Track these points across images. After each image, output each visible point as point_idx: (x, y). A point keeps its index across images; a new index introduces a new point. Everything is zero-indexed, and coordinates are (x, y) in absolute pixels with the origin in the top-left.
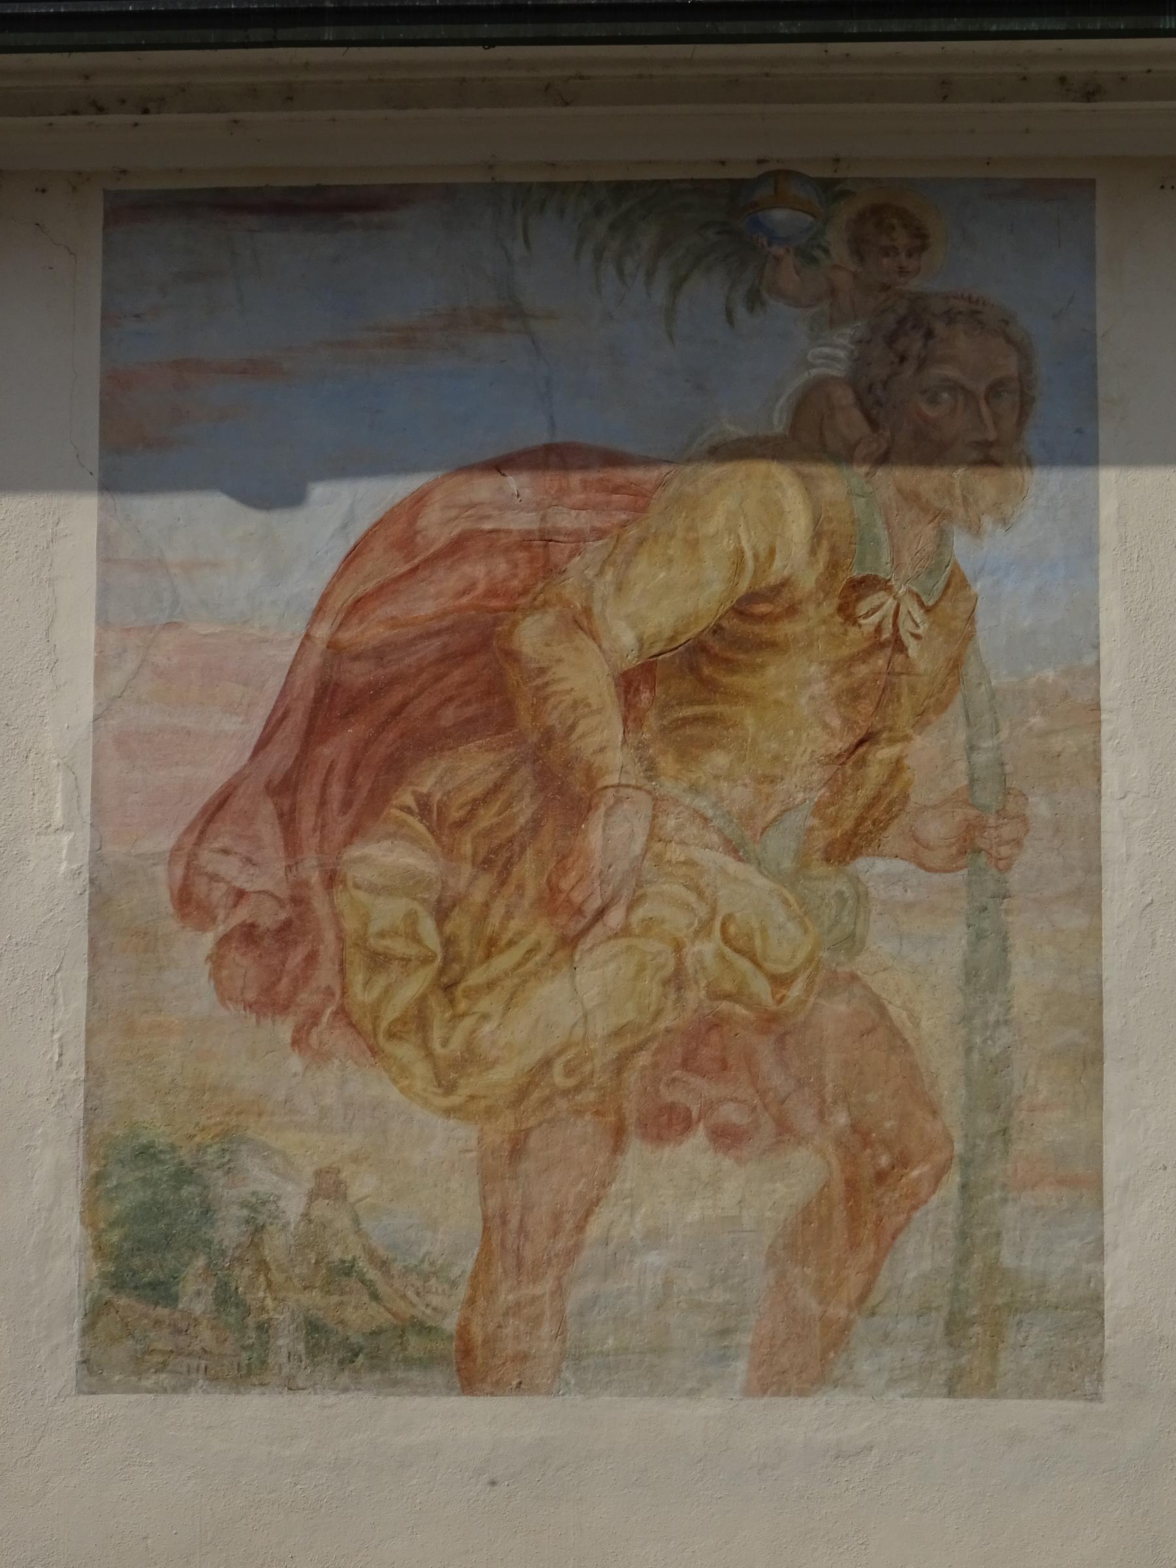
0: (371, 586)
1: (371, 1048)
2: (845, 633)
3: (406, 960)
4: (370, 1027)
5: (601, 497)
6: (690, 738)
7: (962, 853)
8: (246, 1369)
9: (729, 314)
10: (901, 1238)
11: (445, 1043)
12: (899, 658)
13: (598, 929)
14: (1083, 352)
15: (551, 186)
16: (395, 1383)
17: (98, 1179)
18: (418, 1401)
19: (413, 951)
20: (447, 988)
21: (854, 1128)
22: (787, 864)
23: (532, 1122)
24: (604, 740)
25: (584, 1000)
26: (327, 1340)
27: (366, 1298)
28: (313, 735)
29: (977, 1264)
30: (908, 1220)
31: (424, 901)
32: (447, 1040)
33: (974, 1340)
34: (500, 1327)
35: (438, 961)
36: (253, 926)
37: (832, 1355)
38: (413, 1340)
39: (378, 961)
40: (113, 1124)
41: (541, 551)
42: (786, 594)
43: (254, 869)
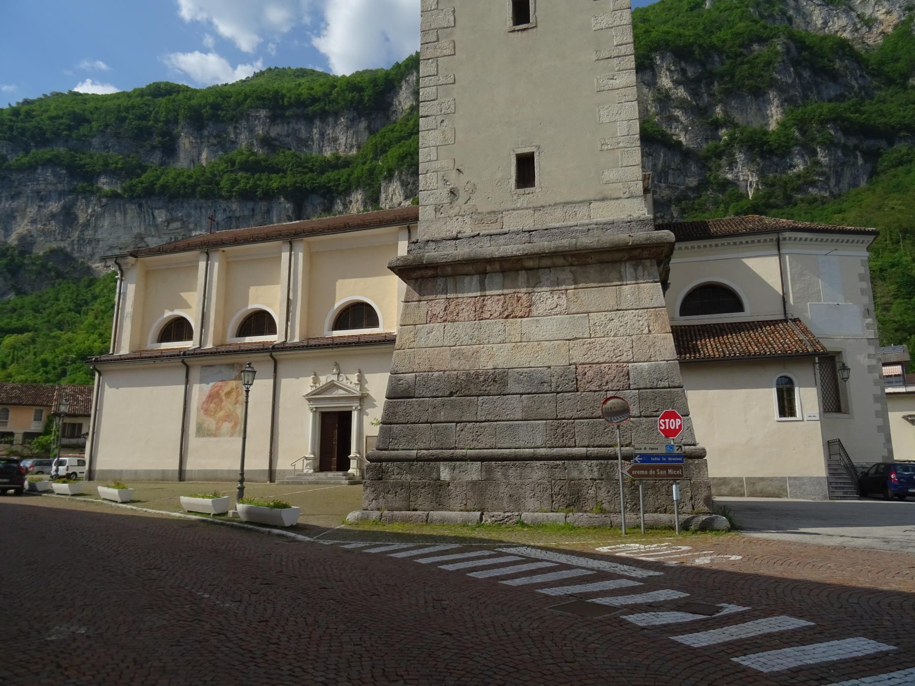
8: (204, 436)
24: (224, 398)
25: (221, 414)
41: (221, 387)
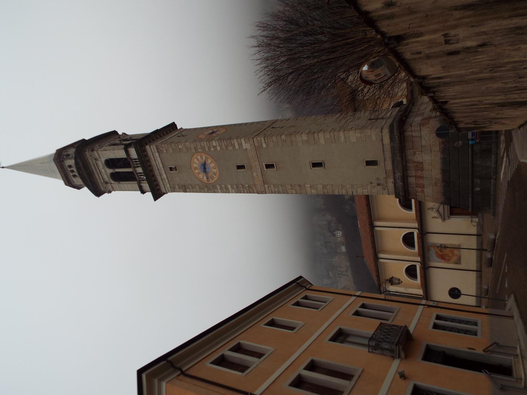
25: (450, 254)
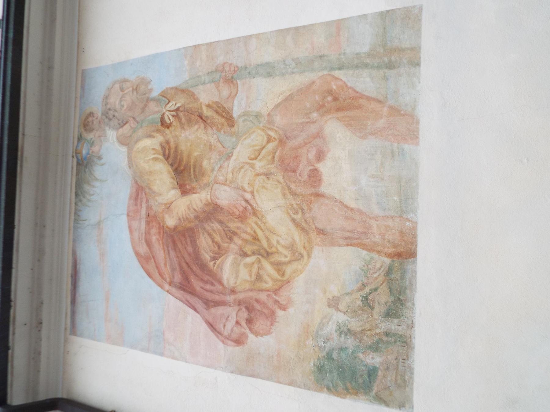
0: (156, 271)
1: (287, 283)
2: (174, 126)
3: (259, 268)
4: (280, 283)
5: (139, 200)
6: (200, 173)
7: (232, 82)
8: (405, 342)
9: (103, 165)
10: (358, 90)
11: (286, 257)
12: (181, 109)
13: (252, 202)
14: (116, 67)
15: (75, 213)
16: (411, 285)
17: (329, 389)
18: (419, 275)
19: (256, 266)
20: (268, 255)
21: (318, 110)
22: (234, 139)
23: (313, 227)
24: (198, 199)
25: (273, 208)
26: (392, 310)
27: (377, 293)
28: (193, 293)
29: (368, 61)
30: (351, 88)
31: (241, 261)
32: (284, 256)
33: (397, 58)
34: (389, 241)
35: (260, 257)
36: (247, 320)
37: (402, 112)
38: (393, 276)
39: (259, 278)
40: (309, 379)
42: (164, 145)
43: (230, 317)
